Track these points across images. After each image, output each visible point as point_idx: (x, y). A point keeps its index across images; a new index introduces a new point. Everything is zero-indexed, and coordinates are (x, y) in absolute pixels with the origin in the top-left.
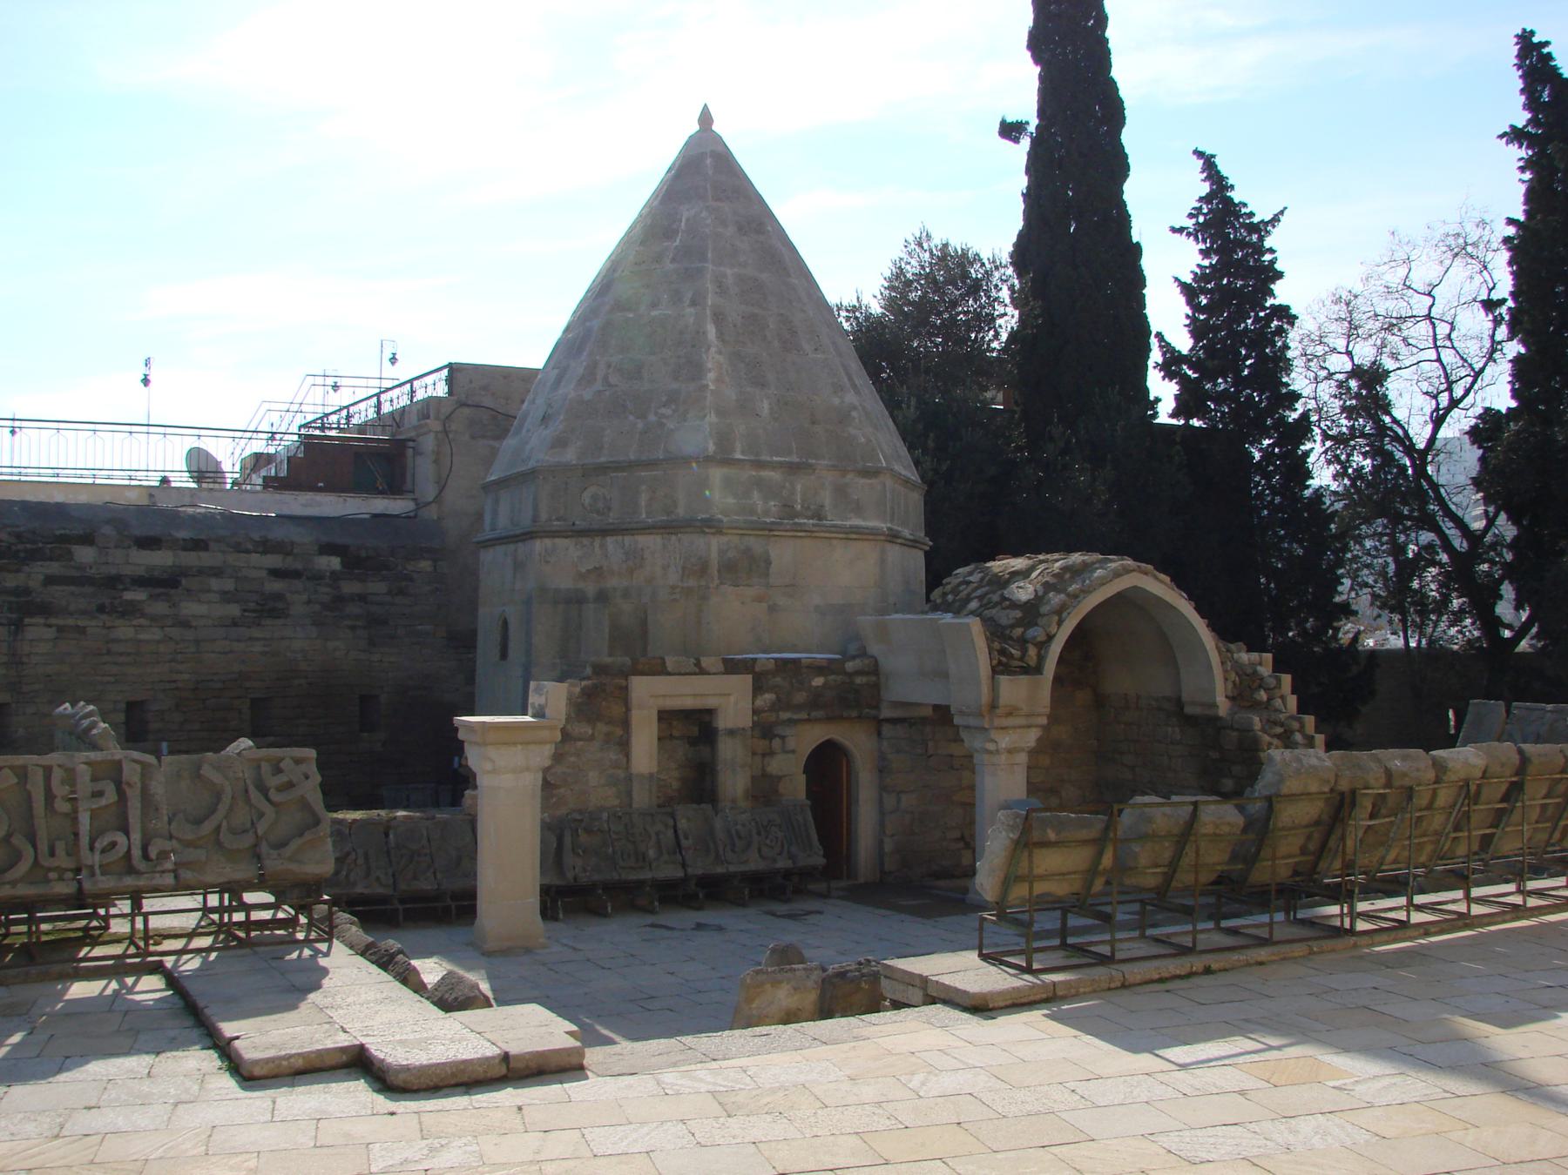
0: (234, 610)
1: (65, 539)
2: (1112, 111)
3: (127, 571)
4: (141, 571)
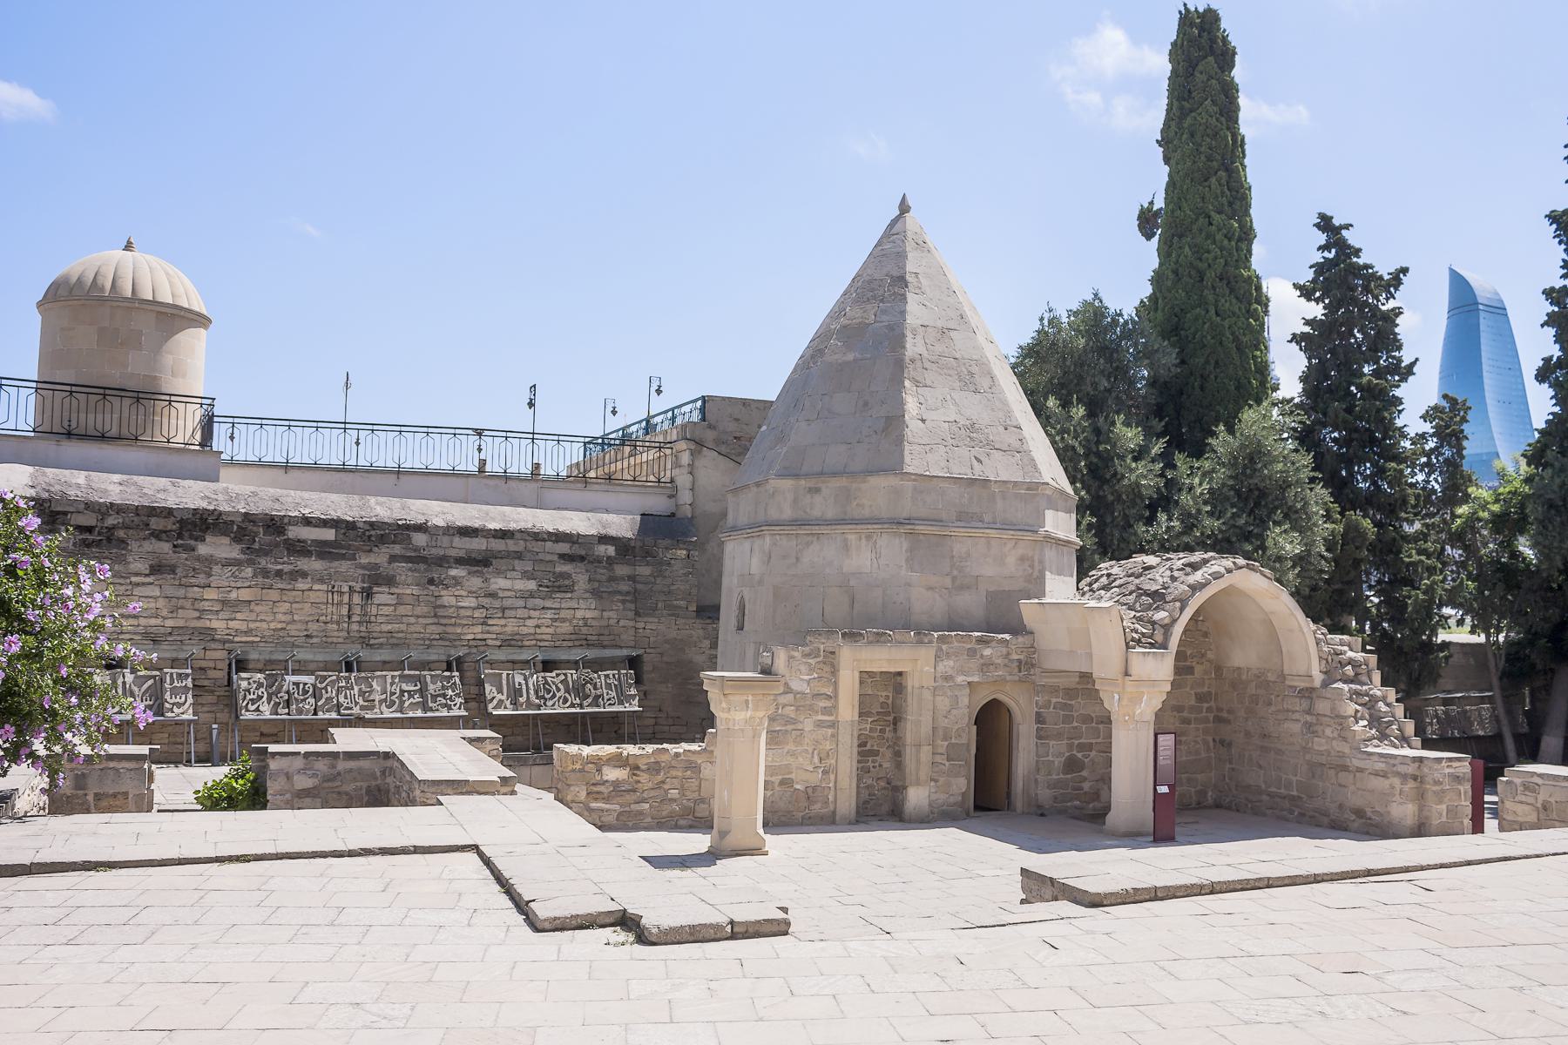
0: (532, 585)
1: (408, 527)
2: (1237, 197)
3: (453, 553)
4: (462, 554)
